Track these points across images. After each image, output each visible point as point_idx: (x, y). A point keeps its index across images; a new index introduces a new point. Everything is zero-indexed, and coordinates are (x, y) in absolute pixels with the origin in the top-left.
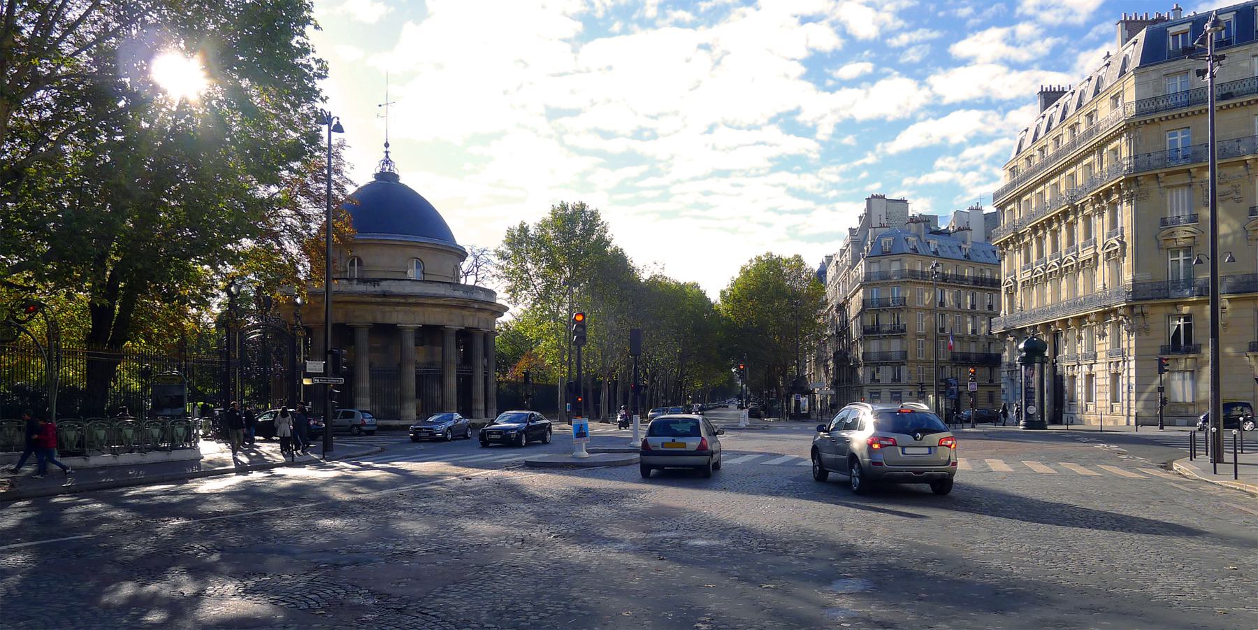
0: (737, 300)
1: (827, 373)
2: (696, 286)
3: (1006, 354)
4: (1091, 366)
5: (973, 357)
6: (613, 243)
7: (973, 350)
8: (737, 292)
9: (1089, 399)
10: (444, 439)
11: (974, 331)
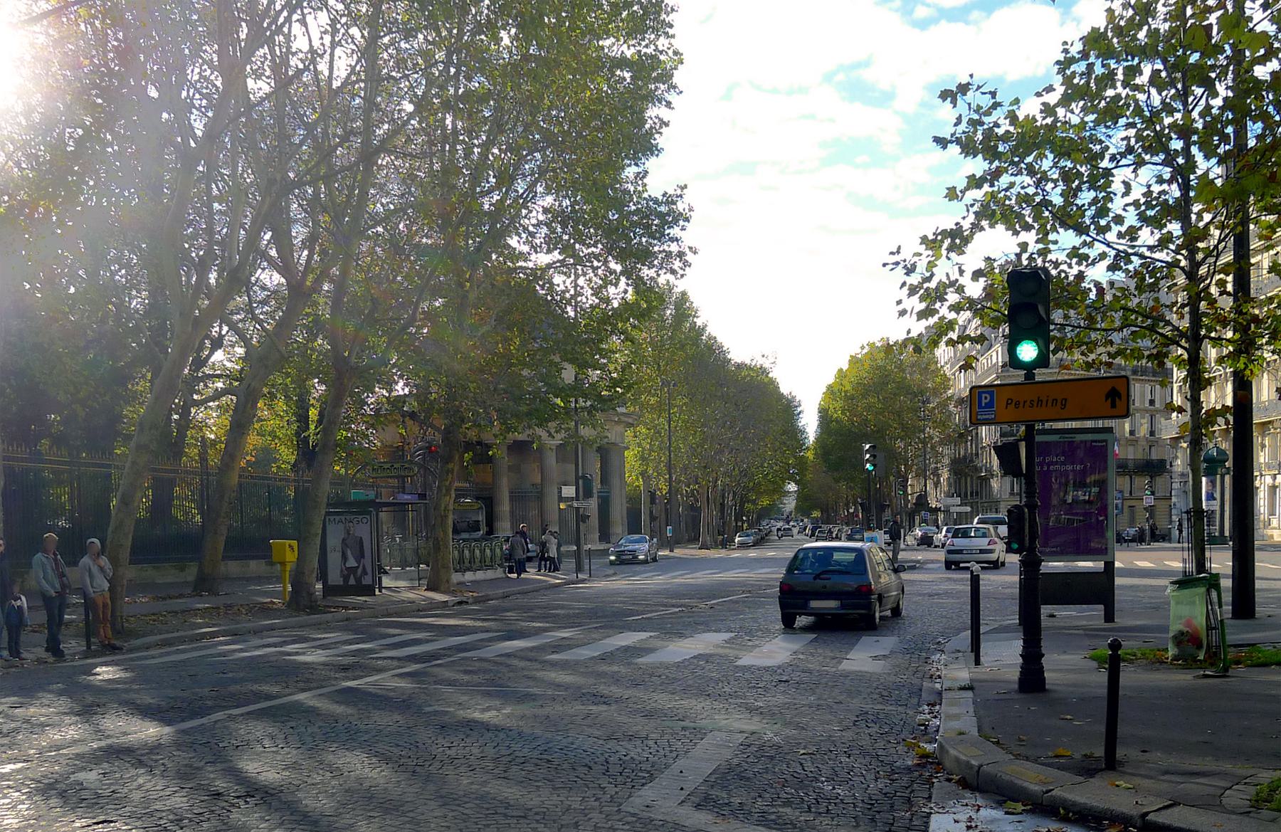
0: (849, 398)
1: (937, 484)
2: (763, 371)
3: (1179, 462)
4: (1274, 477)
5: (1131, 465)
6: (709, 330)
7: (1131, 457)
8: (848, 387)
9: (1272, 513)
10: (645, 562)
11: (1132, 433)
